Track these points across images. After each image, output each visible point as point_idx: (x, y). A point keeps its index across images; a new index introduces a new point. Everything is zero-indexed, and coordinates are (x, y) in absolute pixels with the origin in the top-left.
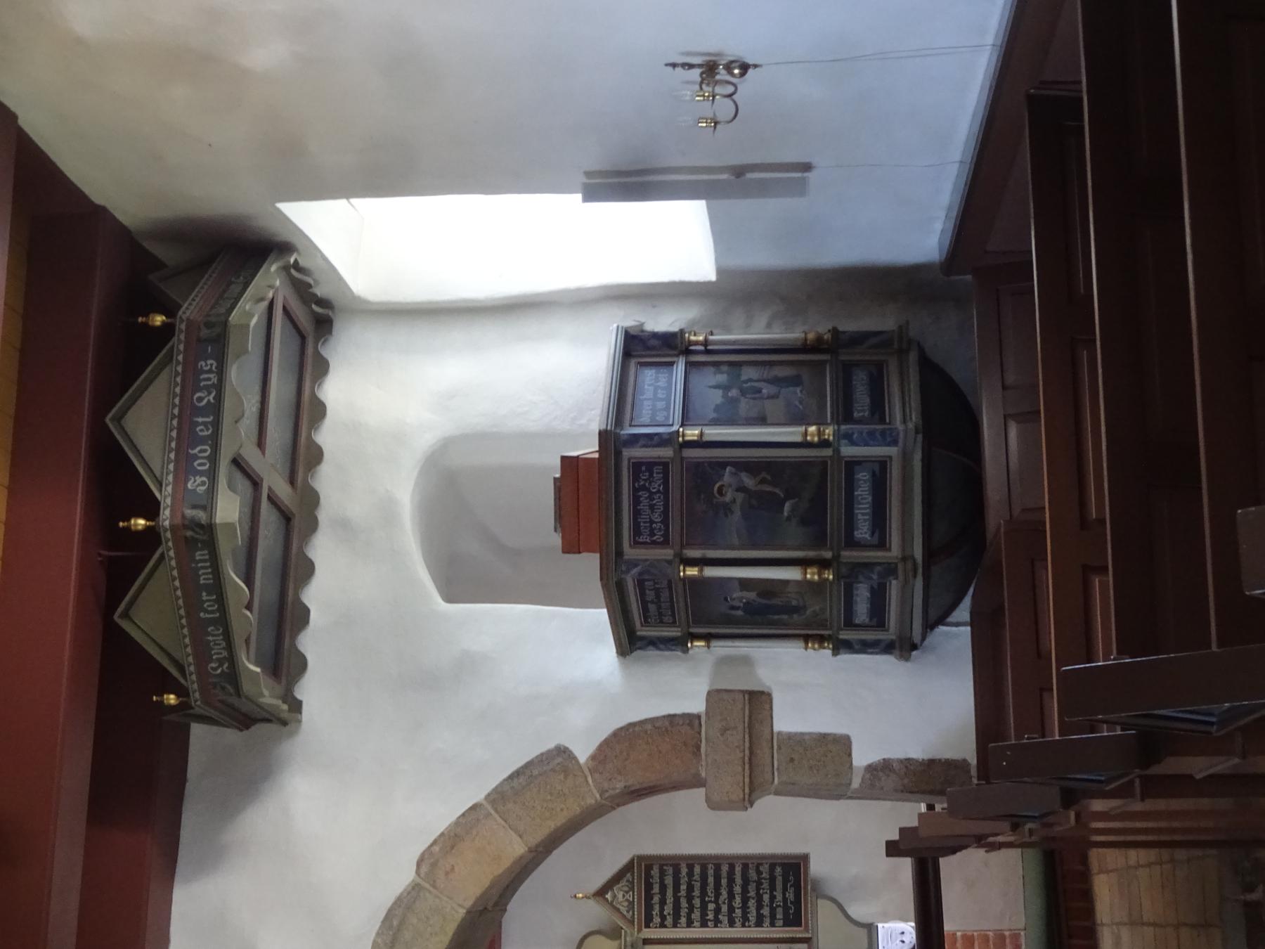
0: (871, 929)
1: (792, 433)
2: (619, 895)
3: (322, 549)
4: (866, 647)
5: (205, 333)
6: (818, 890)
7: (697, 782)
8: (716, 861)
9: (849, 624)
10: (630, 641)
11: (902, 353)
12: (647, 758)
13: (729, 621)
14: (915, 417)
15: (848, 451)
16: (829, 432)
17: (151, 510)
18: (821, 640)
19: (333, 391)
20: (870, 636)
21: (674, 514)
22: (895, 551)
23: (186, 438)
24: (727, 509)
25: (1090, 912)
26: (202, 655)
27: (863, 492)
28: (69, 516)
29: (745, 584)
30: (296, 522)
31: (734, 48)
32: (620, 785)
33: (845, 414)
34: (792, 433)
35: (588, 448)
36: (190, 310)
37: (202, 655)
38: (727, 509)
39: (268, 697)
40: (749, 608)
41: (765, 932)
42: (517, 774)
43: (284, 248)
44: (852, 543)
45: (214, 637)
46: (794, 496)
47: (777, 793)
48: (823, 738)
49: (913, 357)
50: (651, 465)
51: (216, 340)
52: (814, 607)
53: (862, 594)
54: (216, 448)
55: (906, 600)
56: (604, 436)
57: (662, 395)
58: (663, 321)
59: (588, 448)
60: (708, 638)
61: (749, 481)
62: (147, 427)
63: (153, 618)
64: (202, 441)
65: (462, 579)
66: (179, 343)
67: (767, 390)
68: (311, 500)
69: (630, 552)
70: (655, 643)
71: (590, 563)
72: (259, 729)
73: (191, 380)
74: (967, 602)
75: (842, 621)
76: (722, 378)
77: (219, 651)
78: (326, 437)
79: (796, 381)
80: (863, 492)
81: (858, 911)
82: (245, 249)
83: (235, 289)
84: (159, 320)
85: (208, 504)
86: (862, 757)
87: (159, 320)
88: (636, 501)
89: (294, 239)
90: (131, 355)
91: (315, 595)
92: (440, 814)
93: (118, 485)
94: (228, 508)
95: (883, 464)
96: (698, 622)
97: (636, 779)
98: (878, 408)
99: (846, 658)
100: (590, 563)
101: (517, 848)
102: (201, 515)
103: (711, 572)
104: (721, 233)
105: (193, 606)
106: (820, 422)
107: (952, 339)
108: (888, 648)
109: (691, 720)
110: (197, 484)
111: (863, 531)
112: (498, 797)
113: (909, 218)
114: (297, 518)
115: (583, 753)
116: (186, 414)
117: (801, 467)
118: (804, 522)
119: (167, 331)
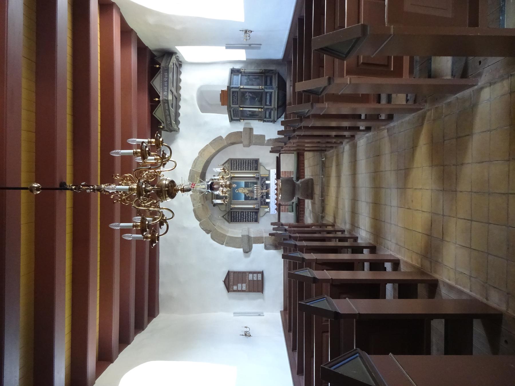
0: (269, 171)
1: (257, 87)
2: (226, 165)
3: (181, 104)
4: (268, 121)
5: (165, 69)
6: (261, 164)
7: (241, 142)
8: (243, 159)
9: (265, 118)
10: (231, 120)
11: (275, 74)
12: (234, 139)
13: (247, 117)
14: (277, 85)
15: (266, 90)
16: (263, 87)
17: (159, 97)
18: (261, 120)
19: (182, 77)
20: (269, 120)
21: (239, 100)
22: (273, 106)
23: (163, 86)
24: (247, 99)
25: (304, 166)
26: (166, 120)
27: (268, 97)
28: (145, 98)
29: (250, 111)
30: (178, 100)
31: (249, 28)
32: (229, 142)
33: (266, 84)
34: (257, 87)
35: (225, 89)
36: (163, 65)
37: (166, 120)
38: (247, 99)
39: (176, 127)
40: (250, 115)
41: (252, 171)
42: (214, 140)
43: (175, 53)
44: (266, 105)
45: (168, 117)
46: (258, 97)
47: (254, 145)
48: (261, 135)
49: (277, 75)
50: (235, 92)
51: (167, 70)
52: (260, 115)
53: (268, 113)
54: (168, 88)
55: (274, 114)
56: (228, 87)
57: (237, 79)
58: (237, 67)
59: (225, 89)
60: (244, 119)
61: (251, 95)
62: (157, 83)
63: (159, 114)
64: (165, 86)
65: (204, 109)
66: (161, 70)
67: (254, 80)
68: (180, 95)
69: (232, 106)
70: (235, 120)
71: (226, 107)
72: (173, 132)
73: (163, 76)
74: (284, 115)
75: (262, 118)
76: (246, 78)
77: (169, 119)
78: (181, 85)
79: (258, 78)
80: (268, 97)
81: (268, 168)
82: (169, 54)
83: (169, 61)
84: (158, 66)
85: (168, 97)
86: (267, 138)
87: (158, 66)
88: (233, 97)
89: (176, 51)
90: (153, 72)
91: (181, 111)
92: (202, 146)
93: (153, 94)
94: (170, 97)
95: (271, 93)
96: (242, 117)
97: (232, 141)
98: (271, 84)
99: (265, 123)
100: (226, 107)
101: (214, 151)
102: (166, 98)
103: (244, 109)
104: (247, 54)
105: (165, 112)
106: (262, 86)
107: (283, 71)
108: (271, 122)
109: (241, 132)
110: (165, 93)
111: (268, 103)
112: (211, 143)
113: (277, 52)
114: (177, 98)
115: (224, 137)
116: (163, 82)
117: (259, 93)
118: (259, 101)
119: (159, 68)
